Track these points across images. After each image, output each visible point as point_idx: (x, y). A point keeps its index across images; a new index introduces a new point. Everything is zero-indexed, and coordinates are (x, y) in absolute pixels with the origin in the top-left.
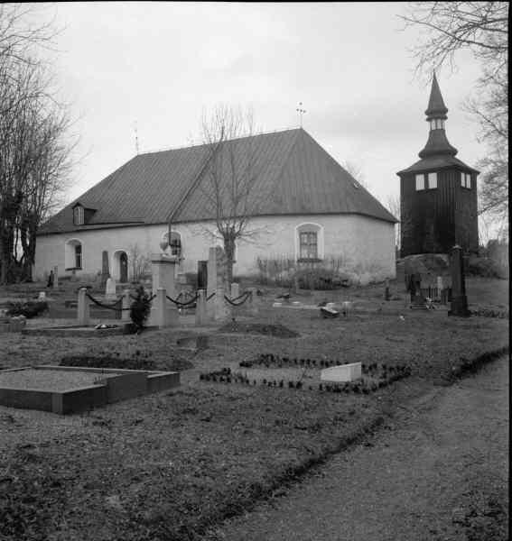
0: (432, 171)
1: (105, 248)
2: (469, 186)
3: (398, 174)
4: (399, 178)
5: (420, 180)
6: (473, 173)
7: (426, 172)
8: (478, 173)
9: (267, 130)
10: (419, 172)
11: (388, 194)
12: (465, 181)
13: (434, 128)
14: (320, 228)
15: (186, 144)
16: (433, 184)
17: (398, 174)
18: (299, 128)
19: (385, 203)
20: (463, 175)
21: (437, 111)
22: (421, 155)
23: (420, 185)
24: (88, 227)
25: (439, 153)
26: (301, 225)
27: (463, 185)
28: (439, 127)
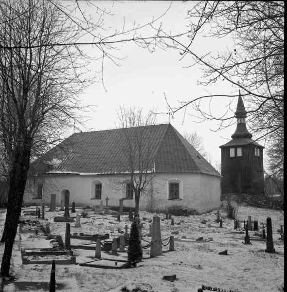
2: (259, 155)
3: (220, 147)
5: (232, 151)
7: (236, 147)
10: (232, 147)
11: (215, 160)
13: (240, 122)
16: (240, 153)
17: (220, 147)
20: (256, 149)
22: (233, 137)
23: (232, 154)
27: (256, 154)
28: (242, 122)
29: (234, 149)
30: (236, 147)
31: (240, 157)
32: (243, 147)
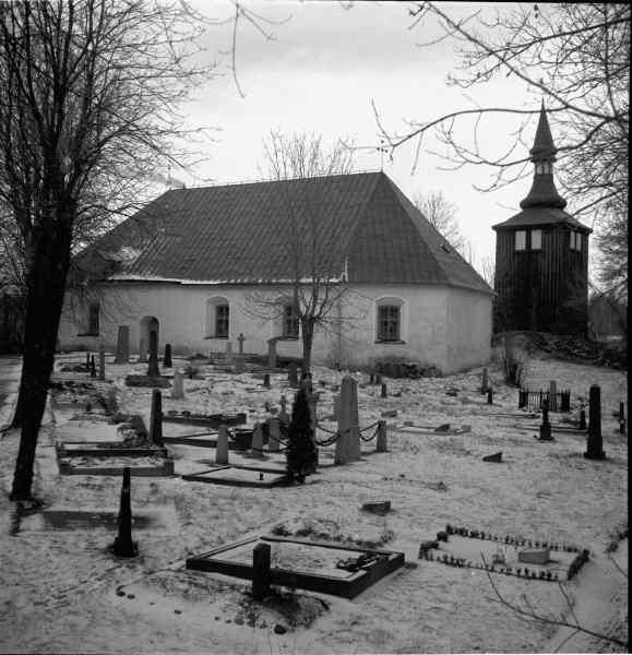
0: (538, 227)
1: (137, 596)
2: (579, 248)
3: (494, 228)
4: (495, 233)
5: (521, 237)
6: (585, 232)
7: (528, 229)
8: (591, 231)
9: (61, 324)
10: (522, 228)
11: (482, 256)
12: (575, 241)
13: (540, 171)
14: (404, 303)
15: (253, 177)
16: (537, 243)
17: (494, 228)
18: (379, 171)
19: (478, 267)
20: (573, 234)
21: (543, 152)
22: (524, 205)
23: (520, 244)
24: (282, 537)
25: (543, 200)
26: (214, 296)
27: (572, 246)
28: (546, 171)
29: (533, 247)
30: (528, 229)
31: (537, 252)
32: (546, 228)
